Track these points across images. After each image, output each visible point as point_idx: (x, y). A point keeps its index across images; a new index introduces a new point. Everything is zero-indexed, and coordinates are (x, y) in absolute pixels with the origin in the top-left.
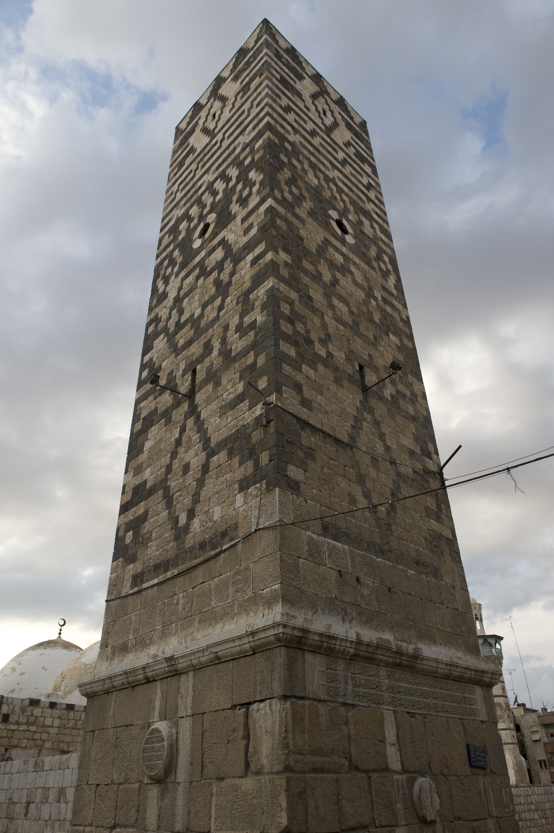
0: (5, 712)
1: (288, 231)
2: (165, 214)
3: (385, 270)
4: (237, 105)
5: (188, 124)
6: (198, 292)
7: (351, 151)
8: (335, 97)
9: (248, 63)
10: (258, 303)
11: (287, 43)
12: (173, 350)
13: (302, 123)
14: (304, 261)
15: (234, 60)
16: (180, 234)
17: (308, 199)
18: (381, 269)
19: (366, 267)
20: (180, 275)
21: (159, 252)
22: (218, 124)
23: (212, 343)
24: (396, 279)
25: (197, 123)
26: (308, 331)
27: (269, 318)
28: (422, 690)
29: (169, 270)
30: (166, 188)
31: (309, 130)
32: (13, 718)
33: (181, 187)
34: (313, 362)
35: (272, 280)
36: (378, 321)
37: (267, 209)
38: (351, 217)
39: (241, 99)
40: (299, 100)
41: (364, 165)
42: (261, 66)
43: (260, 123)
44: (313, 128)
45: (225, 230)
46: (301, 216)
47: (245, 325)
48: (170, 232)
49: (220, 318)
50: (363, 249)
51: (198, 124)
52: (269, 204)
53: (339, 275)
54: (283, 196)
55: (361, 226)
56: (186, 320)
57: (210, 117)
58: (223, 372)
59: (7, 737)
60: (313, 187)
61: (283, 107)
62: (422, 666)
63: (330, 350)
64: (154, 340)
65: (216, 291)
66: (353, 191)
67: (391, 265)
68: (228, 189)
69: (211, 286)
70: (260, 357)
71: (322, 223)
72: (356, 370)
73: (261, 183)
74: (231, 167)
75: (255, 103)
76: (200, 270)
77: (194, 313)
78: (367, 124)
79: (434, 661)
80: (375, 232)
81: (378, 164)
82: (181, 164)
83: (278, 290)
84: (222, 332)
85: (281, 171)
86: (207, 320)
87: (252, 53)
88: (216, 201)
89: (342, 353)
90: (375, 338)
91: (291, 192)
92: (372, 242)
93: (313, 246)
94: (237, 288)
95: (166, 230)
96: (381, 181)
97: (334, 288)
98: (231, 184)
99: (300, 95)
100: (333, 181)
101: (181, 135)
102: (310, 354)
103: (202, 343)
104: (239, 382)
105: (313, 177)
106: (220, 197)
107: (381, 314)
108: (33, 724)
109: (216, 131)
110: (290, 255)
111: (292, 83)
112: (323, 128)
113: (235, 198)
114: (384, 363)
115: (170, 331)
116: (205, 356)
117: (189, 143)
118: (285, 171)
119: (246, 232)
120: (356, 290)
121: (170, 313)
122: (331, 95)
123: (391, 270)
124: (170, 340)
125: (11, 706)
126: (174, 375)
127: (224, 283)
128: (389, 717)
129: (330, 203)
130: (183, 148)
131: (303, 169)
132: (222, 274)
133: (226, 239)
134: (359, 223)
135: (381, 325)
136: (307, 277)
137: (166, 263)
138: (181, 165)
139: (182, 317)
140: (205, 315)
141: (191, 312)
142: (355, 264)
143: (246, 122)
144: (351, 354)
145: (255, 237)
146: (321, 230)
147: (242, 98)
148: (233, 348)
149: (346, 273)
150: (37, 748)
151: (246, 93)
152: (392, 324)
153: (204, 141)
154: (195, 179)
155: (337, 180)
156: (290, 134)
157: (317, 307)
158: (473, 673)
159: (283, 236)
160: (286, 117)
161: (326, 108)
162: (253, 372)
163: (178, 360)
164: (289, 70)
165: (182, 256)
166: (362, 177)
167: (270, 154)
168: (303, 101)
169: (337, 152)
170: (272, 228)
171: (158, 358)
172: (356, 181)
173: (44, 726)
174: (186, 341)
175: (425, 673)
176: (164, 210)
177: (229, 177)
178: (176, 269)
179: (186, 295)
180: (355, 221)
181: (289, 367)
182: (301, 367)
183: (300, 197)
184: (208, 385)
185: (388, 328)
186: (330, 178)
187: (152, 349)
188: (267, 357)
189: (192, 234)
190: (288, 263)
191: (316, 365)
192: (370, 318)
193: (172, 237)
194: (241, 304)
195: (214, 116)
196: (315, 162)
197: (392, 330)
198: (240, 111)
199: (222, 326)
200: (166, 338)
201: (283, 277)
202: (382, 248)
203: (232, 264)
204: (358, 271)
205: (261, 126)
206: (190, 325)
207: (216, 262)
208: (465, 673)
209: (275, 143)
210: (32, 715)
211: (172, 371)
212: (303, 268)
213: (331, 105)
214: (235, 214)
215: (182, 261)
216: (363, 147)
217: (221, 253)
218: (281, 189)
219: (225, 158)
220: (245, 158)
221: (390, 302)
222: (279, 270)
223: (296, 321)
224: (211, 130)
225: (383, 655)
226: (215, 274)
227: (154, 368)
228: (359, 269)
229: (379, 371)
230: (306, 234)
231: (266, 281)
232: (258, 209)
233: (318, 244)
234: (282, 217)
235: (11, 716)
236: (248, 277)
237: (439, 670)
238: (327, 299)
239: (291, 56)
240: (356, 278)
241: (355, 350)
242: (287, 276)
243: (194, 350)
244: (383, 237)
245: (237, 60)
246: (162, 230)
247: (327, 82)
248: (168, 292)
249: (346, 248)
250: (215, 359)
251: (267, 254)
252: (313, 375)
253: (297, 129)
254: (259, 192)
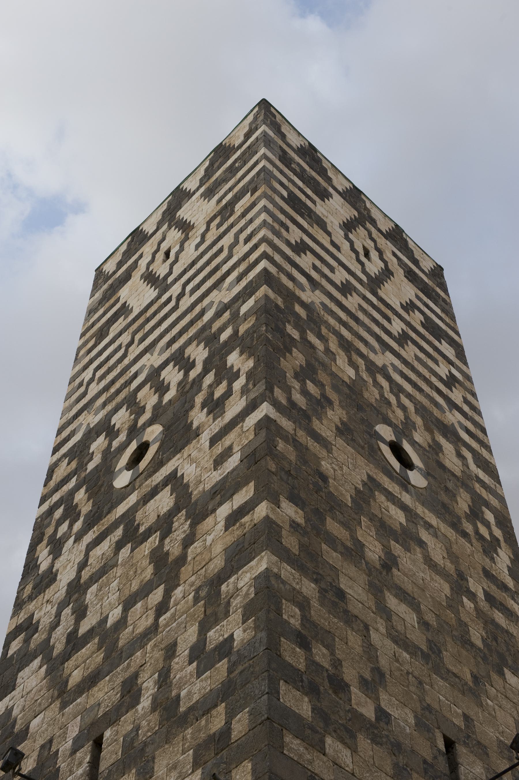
1: (298, 463)
2: (64, 420)
3: (488, 537)
4: (210, 238)
5: (120, 265)
6: (118, 574)
7: (416, 318)
8: (385, 226)
9: (232, 170)
10: (236, 602)
11: (301, 138)
12: (56, 693)
13: (326, 271)
14: (329, 520)
15: (207, 163)
16: (91, 459)
17: (336, 403)
18: (481, 538)
19: (451, 533)
20: (85, 538)
21: (46, 491)
22: (175, 267)
23: (139, 681)
24: (512, 556)
25: (136, 264)
26: (337, 664)
27: (259, 635)
29: (64, 528)
30: (69, 373)
31: (339, 284)
33: (99, 374)
34: (348, 730)
35: (265, 558)
36: (479, 643)
37: (259, 421)
38: (417, 437)
39: (217, 229)
40: (321, 232)
41: (440, 342)
42: (254, 176)
43: (250, 271)
44: (346, 280)
45: (178, 456)
46: (323, 434)
47: (210, 646)
48: (71, 455)
49: (160, 630)
50: (444, 497)
51: (137, 267)
52: (263, 414)
53: (397, 549)
54: (289, 399)
55: (437, 454)
56: (89, 631)
57: (160, 256)
58: (159, 747)
60: (346, 383)
61: (292, 244)
63: (383, 705)
64: (20, 670)
65: (155, 574)
66: (420, 390)
67: (500, 529)
68: (187, 383)
69: (146, 562)
70: (239, 716)
71: (363, 448)
72: (439, 751)
73: (250, 375)
74: (195, 343)
75: (242, 237)
76: (124, 530)
77: (107, 617)
78: (445, 272)
80: (466, 465)
81: (466, 342)
82: (102, 334)
83: (278, 576)
84: (162, 659)
85: (287, 354)
86: (133, 632)
87: (239, 153)
88: (164, 403)
89: (407, 711)
90: (475, 678)
91: (304, 392)
92: (459, 484)
93: (346, 491)
94: (196, 569)
95: (64, 450)
96: (473, 371)
97: (387, 573)
98: (193, 374)
99: (322, 224)
100: (383, 371)
101: (105, 282)
102: (342, 714)
103: (119, 680)
104: (193, 772)
105: (347, 365)
106: (172, 396)
107: (484, 628)
109: (170, 279)
110: (302, 509)
111: (309, 203)
112: (364, 279)
113: (199, 399)
114: (498, 735)
115: (56, 653)
116: (124, 709)
117: (119, 298)
118: (294, 354)
119: (219, 462)
120: (432, 579)
121: (58, 615)
122: (378, 222)
123: (501, 539)
124: (53, 670)
126: (54, 749)
127: (171, 558)
129: (378, 411)
130: (107, 305)
131: (327, 350)
132: (167, 541)
133: (179, 474)
134: (433, 449)
135: (486, 651)
136: (335, 551)
137: (59, 513)
138: (101, 334)
139: (82, 623)
140: (130, 622)
141: (101, 614)
142: (428, 526)
143: (225, 268)
144: (427, 713)
145: (235, 473)
146: (361, 461)
147: (219, 226)
148: (183, 693)
149: (412, 544)
151: (227, 220)
152: (508, 650)
153: (147, 295)
154: (126, 361)
155: (390, 370)
156: (303, 290)
157: (356, 612)
159: (288, 473)
160: (297, 262)
161: (370, 245)
162: (222, 750)
163: (66, 715)
164: (304, 183)
165: (91, 501)
166: (438, 365)
167: (267, 325)
168: (329, 234)
169: (389, 320)
170: (268, 458)
171: (23, 710)
172: (426, 371)
174: (86, 674)
176: (63, 414)
177: (191, 360)
178: (78, 526)
179: (94, 579)
180: (425, 445)
181: (298, 741)
182: (323, 742)
183: (322, 400)
184: (126, 776)
185: (502, 657)
186: (377, 366)
187: (14, 689)
188: (252, 716)
189: (114, 461)
190: (298, 525)
191: (353, 737)
192: (462, 636)
193: (74, 464)
194: (203, 602)
195: (167, 254)
196: (349, 339)
197: (510, 662)
198: (215, 249)
199: (163, 646)
200: (45, 667)
201: (287, 551)
202: (480, 497)
203: (188, 523)
204: (434, 540)
205: (252, 275)
206: (96, 640)
207: (158, 516)
209: (277, 306)
211: (51, 741)
212: (327, 533)
213: (378, 241)
214: (198, 428)
215: (91, 511)
216: (438, 311)
217: (168, 500)
218: (288, 385)
219: (184, 327)
220: (222, 330)
221: (501, 604)
222: (281, 537)
223: (314, 642)
224: (161, 277)
226: (154, 540)
227: (13, 732)
228: (437, 537)
229: (487, 755)
230: (332, 468)
231: (254, 558)
232: (243, 420)
233: (356, 488)
234: (287, 437)
236: (218, 548)
238: (375, 596)
239: (308, 159)
240: (432, 554)
241: (436, 706)
242: (295, 550)
243: (100, 695)
244: (481, 474)
245: (212, 164)
246: (56, 450)
247: (372, 202)
248: (58, 571)
249: (411, 495)
250: (144, 716)
251: (257, 505)
252: (348, 761)
253: (317, 282)
254: (244, 391)
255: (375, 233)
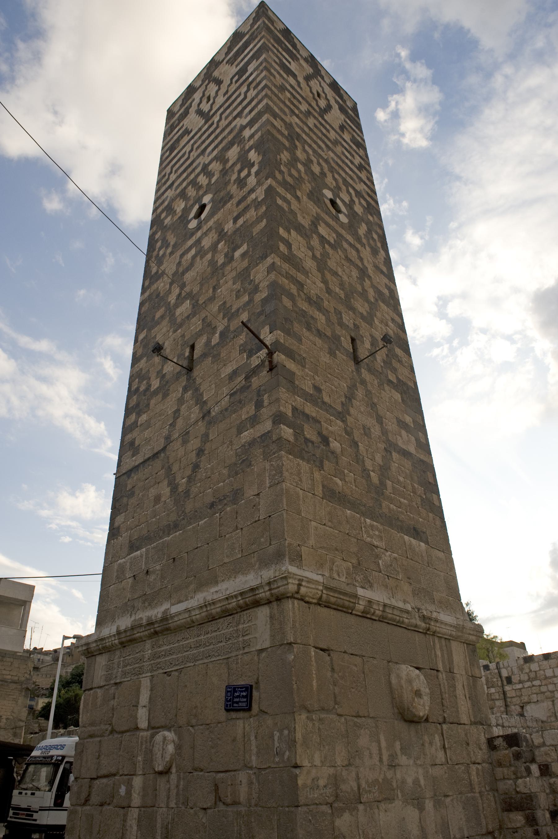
0: (507, 675)
5: (182, 106)
25: (190, 105)
28: (183, 645)
29: (161, 253)
32: (515, 679)
57: (205, 101)
59: (517, 696)
62: (175, 624)
79: (185, 612)
82: (172, 149)
108: (536, 678)
125: (509, 669)
128: (146, 683)
150: (549, 700)
158: (240, 598)
173: (546, 678)
175: (180, 629)
208: (229, 604)
210: (531, 671)
213: (324, 87)
225: (138, 633)
226: (209, 256)
235: (513, 677)
237: (194, 617)
254: (257, 174)
255: (323, 84)
